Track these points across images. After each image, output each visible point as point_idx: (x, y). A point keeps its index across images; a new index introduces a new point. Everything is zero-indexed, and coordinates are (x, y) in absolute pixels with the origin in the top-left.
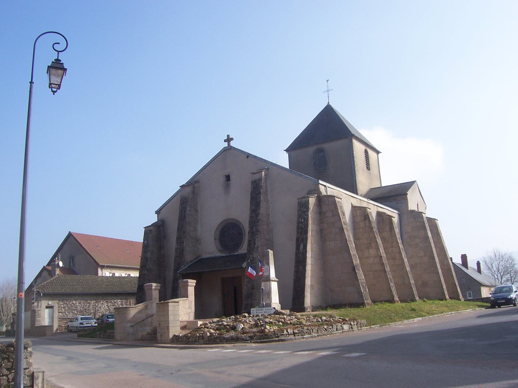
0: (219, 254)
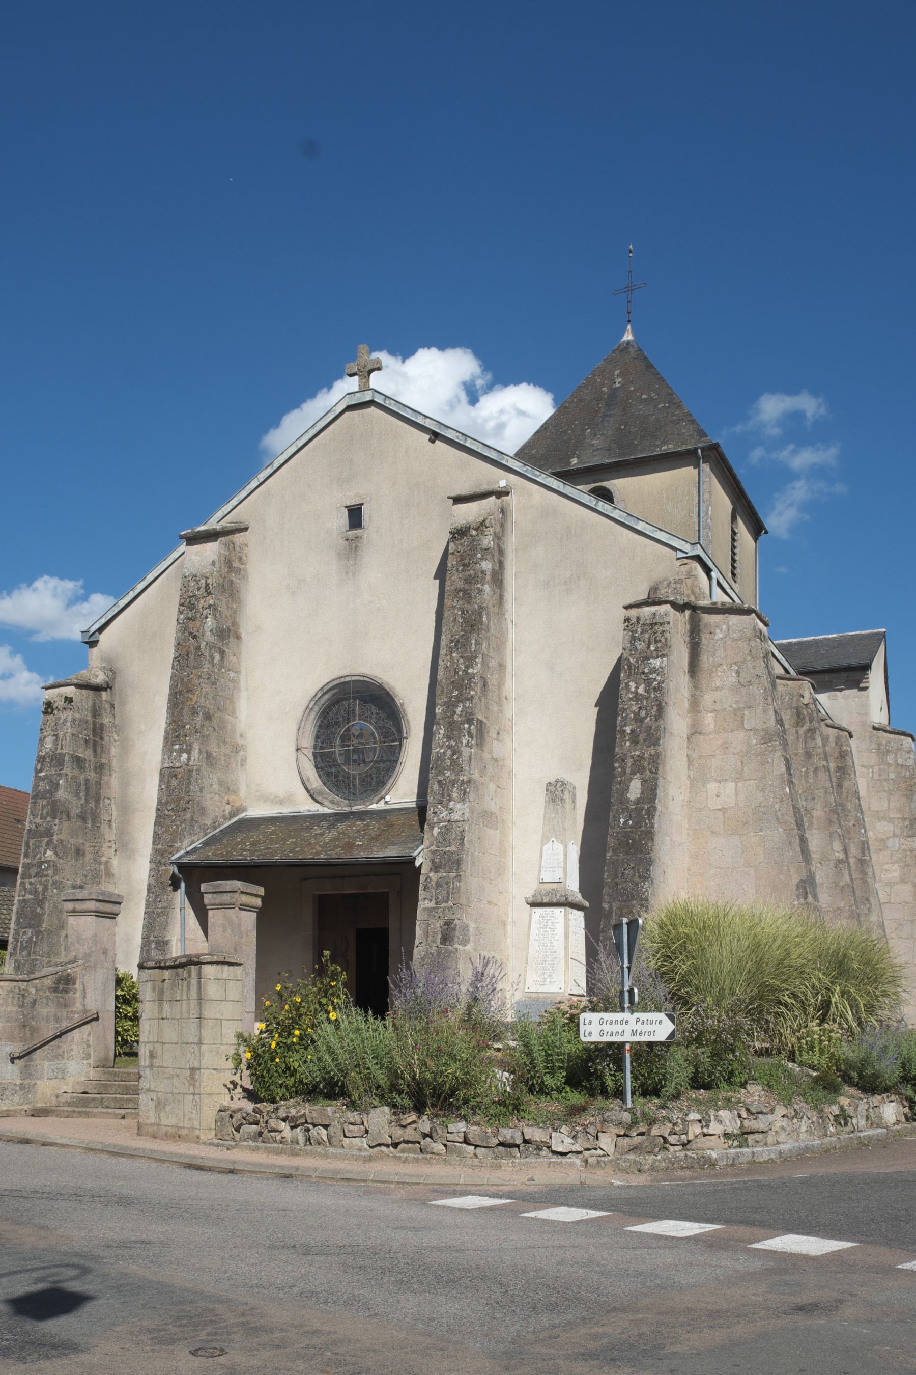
0: (307, 806)
